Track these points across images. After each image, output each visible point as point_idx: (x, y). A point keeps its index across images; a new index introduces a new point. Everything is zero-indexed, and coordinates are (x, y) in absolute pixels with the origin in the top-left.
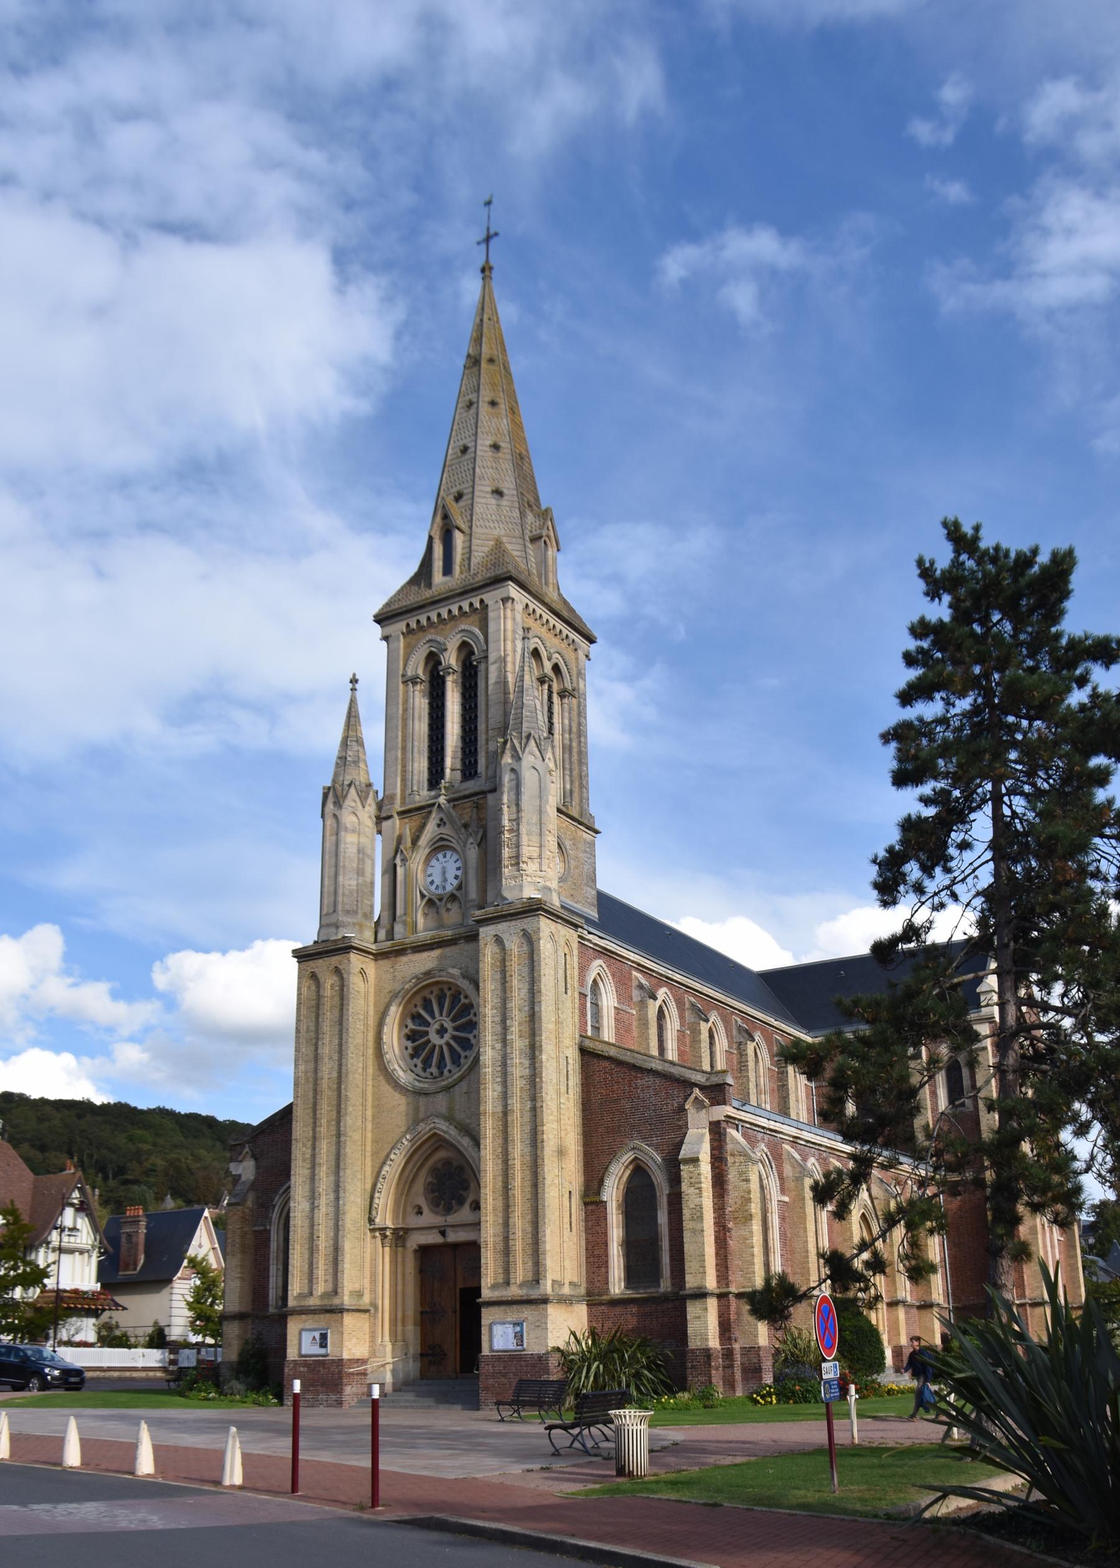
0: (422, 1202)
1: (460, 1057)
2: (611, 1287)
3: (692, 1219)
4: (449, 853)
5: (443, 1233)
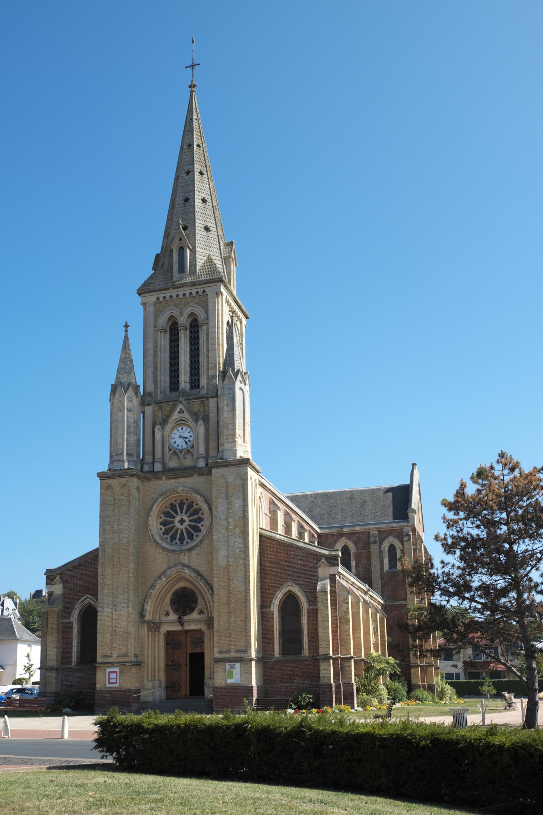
4: (185, 428)
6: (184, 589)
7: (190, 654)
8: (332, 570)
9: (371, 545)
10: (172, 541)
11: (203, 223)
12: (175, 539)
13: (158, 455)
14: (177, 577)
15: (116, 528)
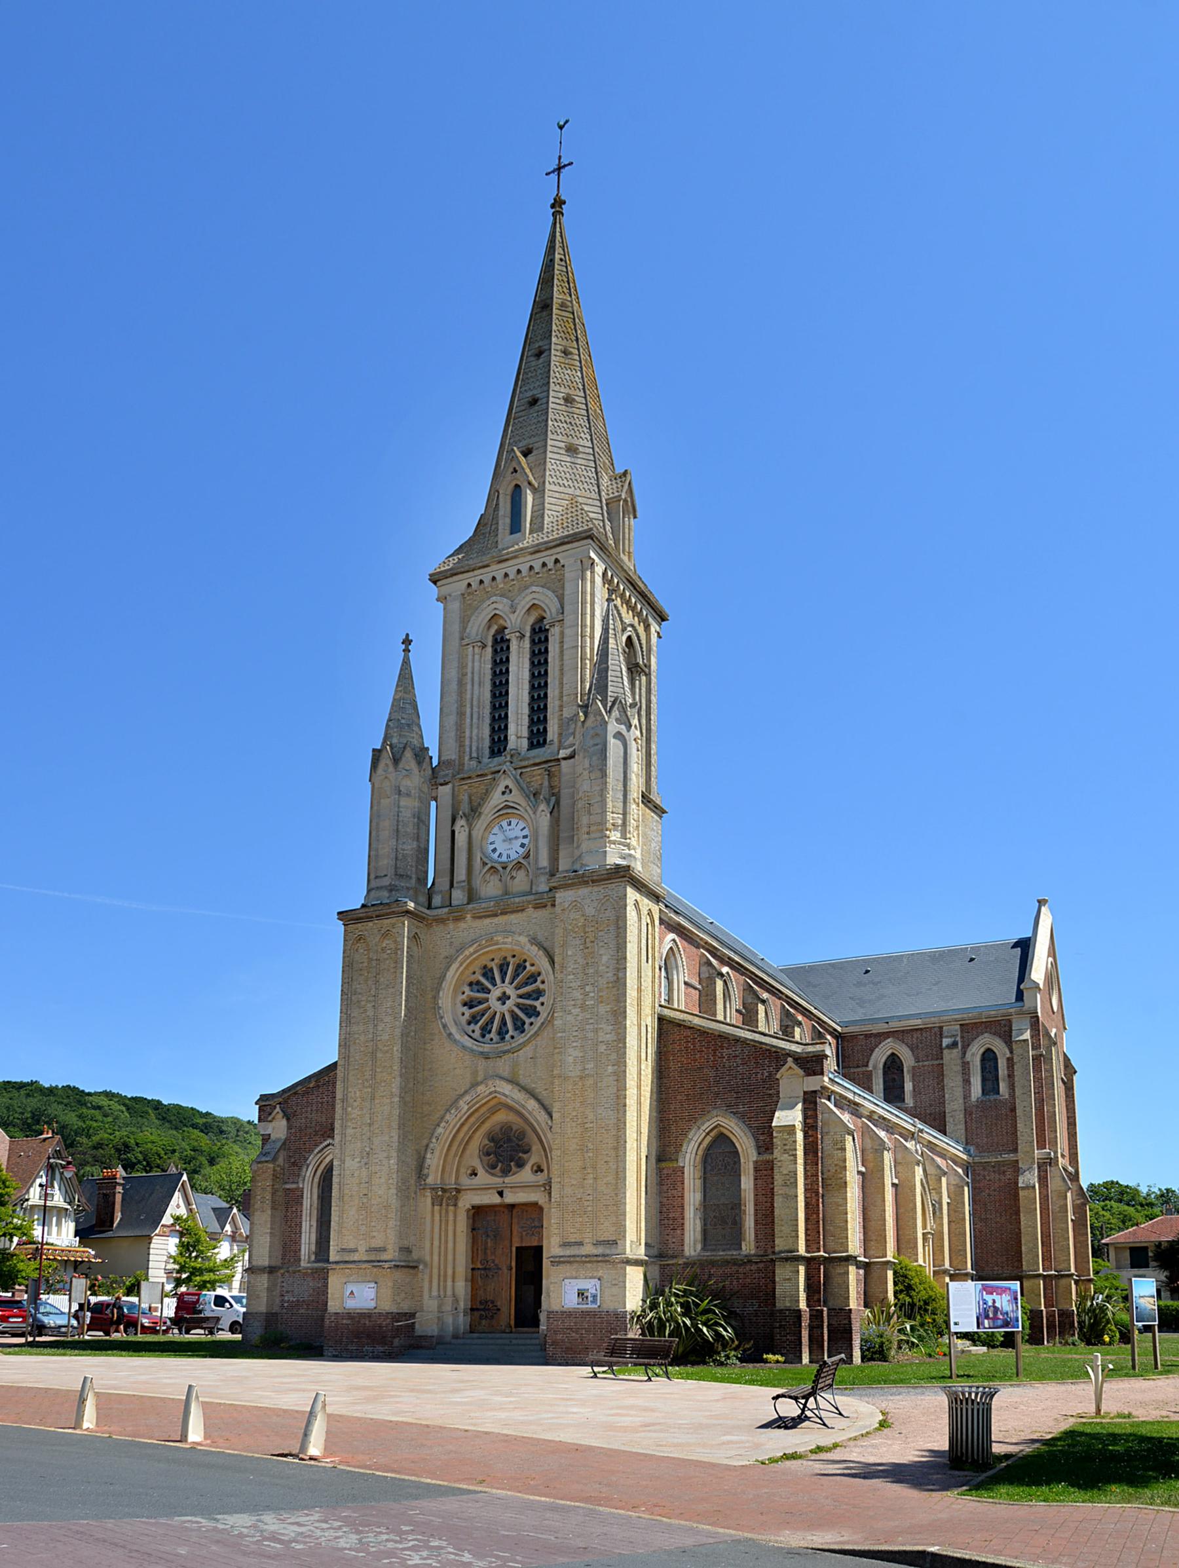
1: (524, 1023)
2: (686, 1248)
3: (785, 1185)
5: (501, 1194)
6: (506, 1129)
7: (517, 1248)
8: (812, 1083)
9: (945, 1052)
10: (483, 1036)
11: (564, 438)
12: (490, 1032)
13: (461, 874)
14: (492, 1103)
15: (370, 1013)
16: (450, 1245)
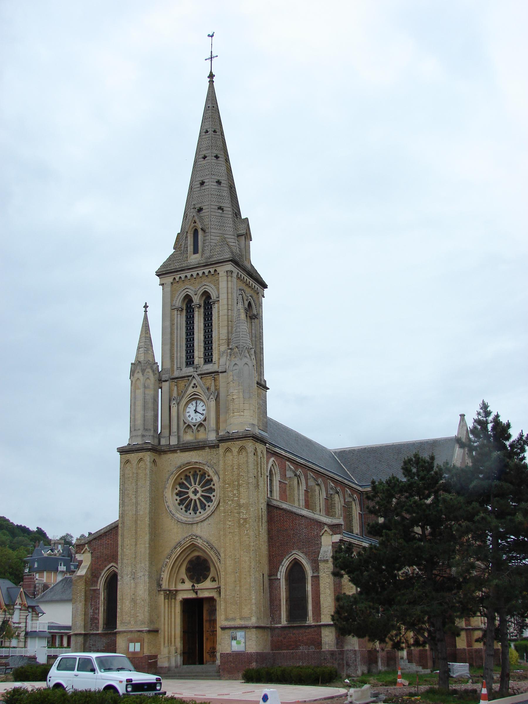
0: (185, 577)
4: (199, 402)
16: (173, 620)
